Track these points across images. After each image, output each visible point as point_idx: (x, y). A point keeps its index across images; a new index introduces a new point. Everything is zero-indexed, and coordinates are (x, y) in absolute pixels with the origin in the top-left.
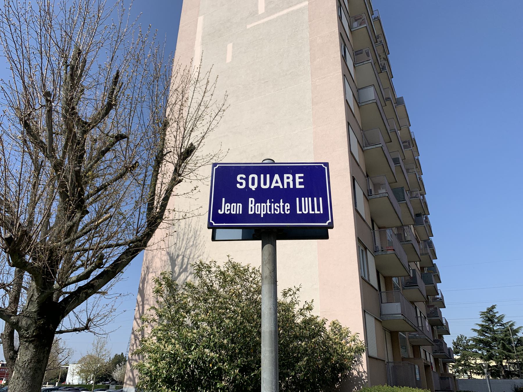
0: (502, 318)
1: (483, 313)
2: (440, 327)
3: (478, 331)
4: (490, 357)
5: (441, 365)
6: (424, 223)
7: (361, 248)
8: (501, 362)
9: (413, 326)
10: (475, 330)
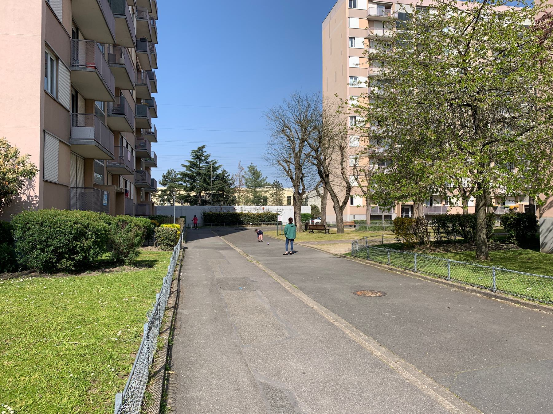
0: (208, 157)
1: (194, 152)
2: (146, 160)
3: (187, 166)
4: (192, 189)
5: (142, 194)
6: (148, 50)
7: (50, 56)
8: (200, 193)
9: (109, 154)
10: (184, 166)
